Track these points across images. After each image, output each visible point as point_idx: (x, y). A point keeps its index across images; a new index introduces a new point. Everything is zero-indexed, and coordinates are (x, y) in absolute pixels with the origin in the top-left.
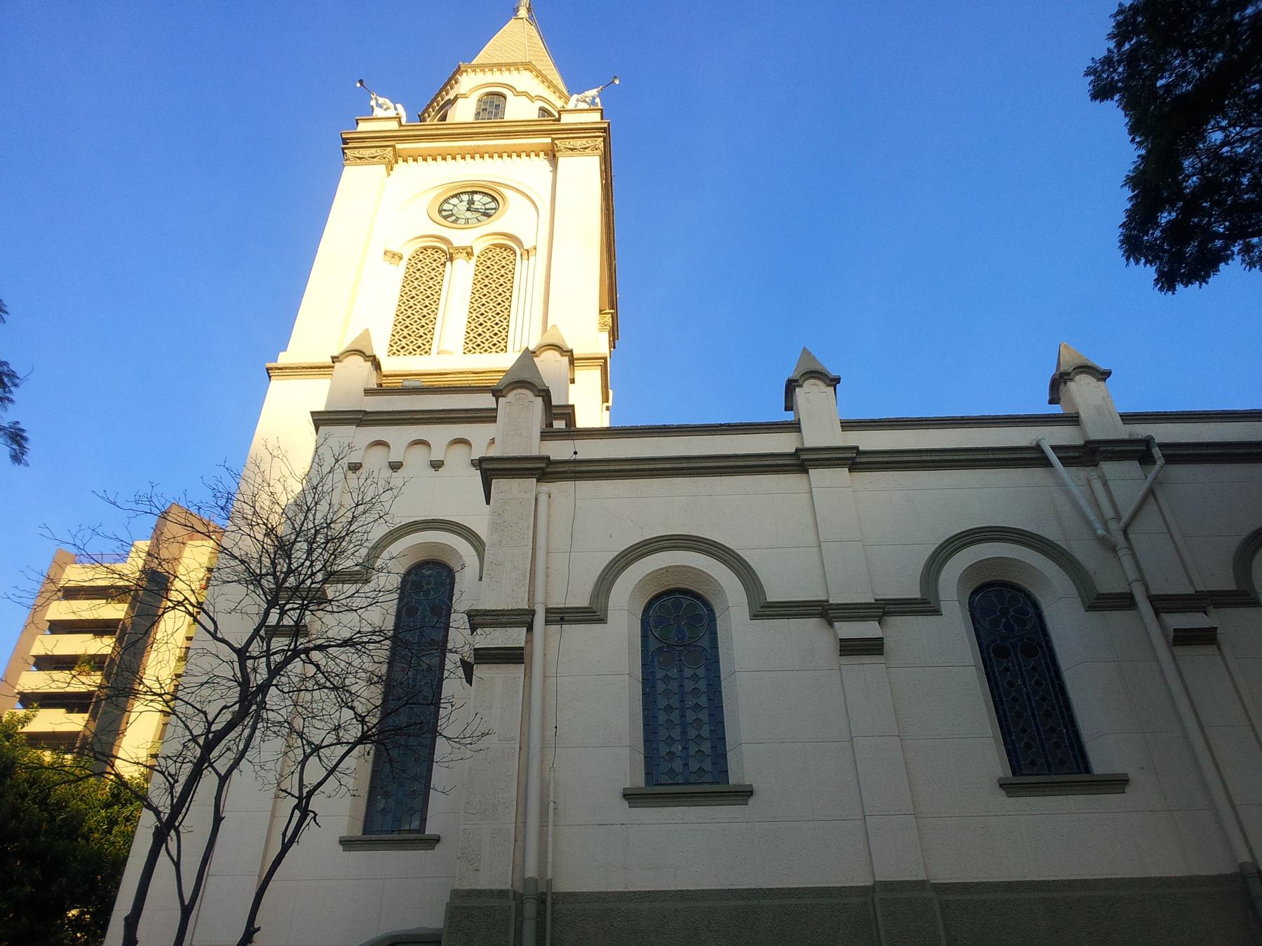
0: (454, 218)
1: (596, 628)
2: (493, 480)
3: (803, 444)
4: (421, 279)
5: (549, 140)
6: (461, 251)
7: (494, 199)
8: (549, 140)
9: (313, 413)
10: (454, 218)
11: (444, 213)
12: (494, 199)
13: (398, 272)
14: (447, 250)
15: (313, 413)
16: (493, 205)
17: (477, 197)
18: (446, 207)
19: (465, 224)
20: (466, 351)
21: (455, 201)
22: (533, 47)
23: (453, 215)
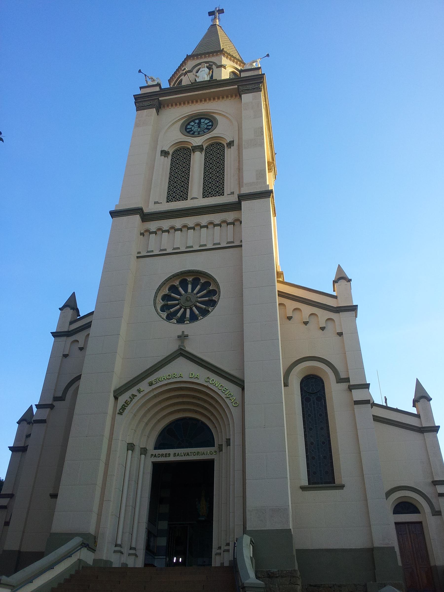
0: (193, 132)
1: (333, 291)
2: (242, 95)
3: (422, 425)
4: (179, 168)
5: (236, 86)
6: (198, 148)
7: (211, 121)
8: (236, 86)
9: (134, 96)
10: (193, 132)
11: (188, 130)
12: (211, 121)
13: (168, 161)
14: (191, 148)
15: (134, 96)
16: (210, 124)
17: (202, 121)
18: (189, 127)
19: (198, 134)
20: (204, 196)
21: (192, 123)
22: (222, 37)
23: (192, 131)
